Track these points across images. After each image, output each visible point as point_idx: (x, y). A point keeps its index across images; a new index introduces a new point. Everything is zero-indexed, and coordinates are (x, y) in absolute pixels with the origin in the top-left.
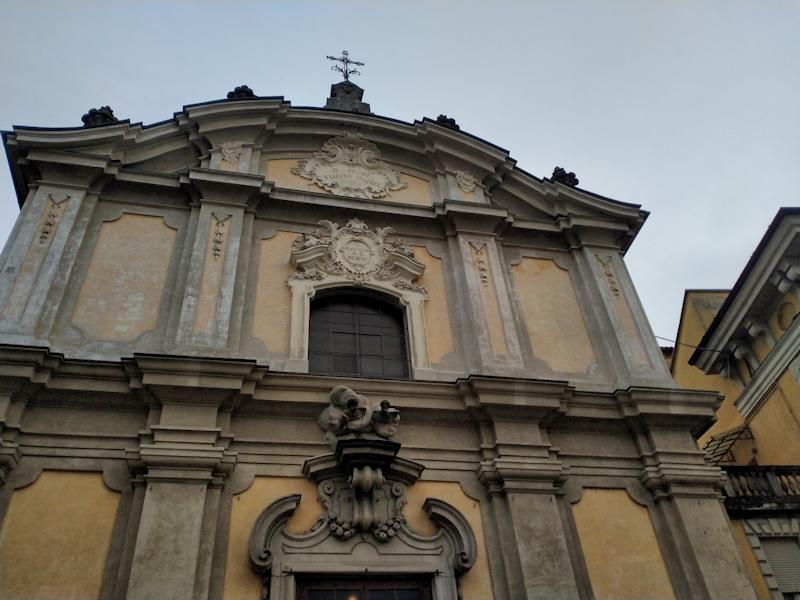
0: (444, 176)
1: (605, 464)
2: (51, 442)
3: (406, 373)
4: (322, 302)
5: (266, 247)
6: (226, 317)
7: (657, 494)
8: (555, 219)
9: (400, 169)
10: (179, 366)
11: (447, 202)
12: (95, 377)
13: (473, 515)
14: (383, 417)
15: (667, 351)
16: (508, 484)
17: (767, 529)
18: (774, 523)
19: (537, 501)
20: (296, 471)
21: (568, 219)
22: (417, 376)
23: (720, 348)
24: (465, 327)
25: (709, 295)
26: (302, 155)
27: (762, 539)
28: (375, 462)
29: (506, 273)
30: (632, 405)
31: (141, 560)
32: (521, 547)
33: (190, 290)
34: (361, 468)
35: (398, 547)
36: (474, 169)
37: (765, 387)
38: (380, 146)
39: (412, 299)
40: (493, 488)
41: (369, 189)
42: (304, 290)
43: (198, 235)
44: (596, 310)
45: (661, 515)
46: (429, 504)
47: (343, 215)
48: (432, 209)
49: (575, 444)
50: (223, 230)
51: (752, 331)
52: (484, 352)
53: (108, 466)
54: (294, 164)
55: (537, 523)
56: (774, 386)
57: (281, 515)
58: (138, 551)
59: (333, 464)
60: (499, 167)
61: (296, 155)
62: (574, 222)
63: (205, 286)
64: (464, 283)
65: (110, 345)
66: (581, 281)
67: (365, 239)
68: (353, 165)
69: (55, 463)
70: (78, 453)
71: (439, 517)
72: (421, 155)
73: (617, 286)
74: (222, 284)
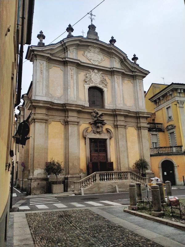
0: (113, 58)
1: (132, 123)
2: (52, 116)
3: (102, 106)
4: (90, 89)
5: (79, 75)
6: (76, 94)
7: (139, 128)
8: (133, 72)
9: (103, 54)
10: (72, 106)
11: (113, 68)
12: (58, 106)
13: (113, 130)
14: (102, 115)
15: (145, 92)
16: (118, 126)
17: (153, 133)
18: (154, 132)
19: (122, 129)
20: (88, 123)
21: (135, 72)
22: (106, 108)
23: (154, 99)
24: (114, 96)
25: (156, 85)
26: (85, 50)
27: (152, 134)
28: (101, 123)
29: (122, 86)
30: (139, 114)
31: (70, 135)
32: (119, 136)
33: (69, 87)
34: (98, 124)
35: (102, 135)
36: (119, 58)
37: (160, 108)
38: (100, 48)
39: (105, 89)
40: (116, 127)
41: (98, 61)
42: (87, 87)
43: (68, 74)
44: (136, 93)
45: (139, 131)
46: (107, 129)
47: (93, 69)
48: (110, 68)
49: (129, 120)
50: (72, 73)
51: (161, 99)
52: (117, 102)
53: (61, 121)
54: (82, 52)
55: (122, 132)
56: (161, 109)
57: (87, 129)
58: (69, 135)
59: (94, 122)
60: (124, 58)
61: (83, 50)
62: (136, 74)
63: (71, 87)
64: (115, 87)
65: (57, 98)
66: (135, 86)
67: (97, 74)
68: (94, 53)
69: (54, 120)
70: (56, 118)
71: (108, 131)
72: (108, 52)
73: (141, 89)
74: (74, 86)
